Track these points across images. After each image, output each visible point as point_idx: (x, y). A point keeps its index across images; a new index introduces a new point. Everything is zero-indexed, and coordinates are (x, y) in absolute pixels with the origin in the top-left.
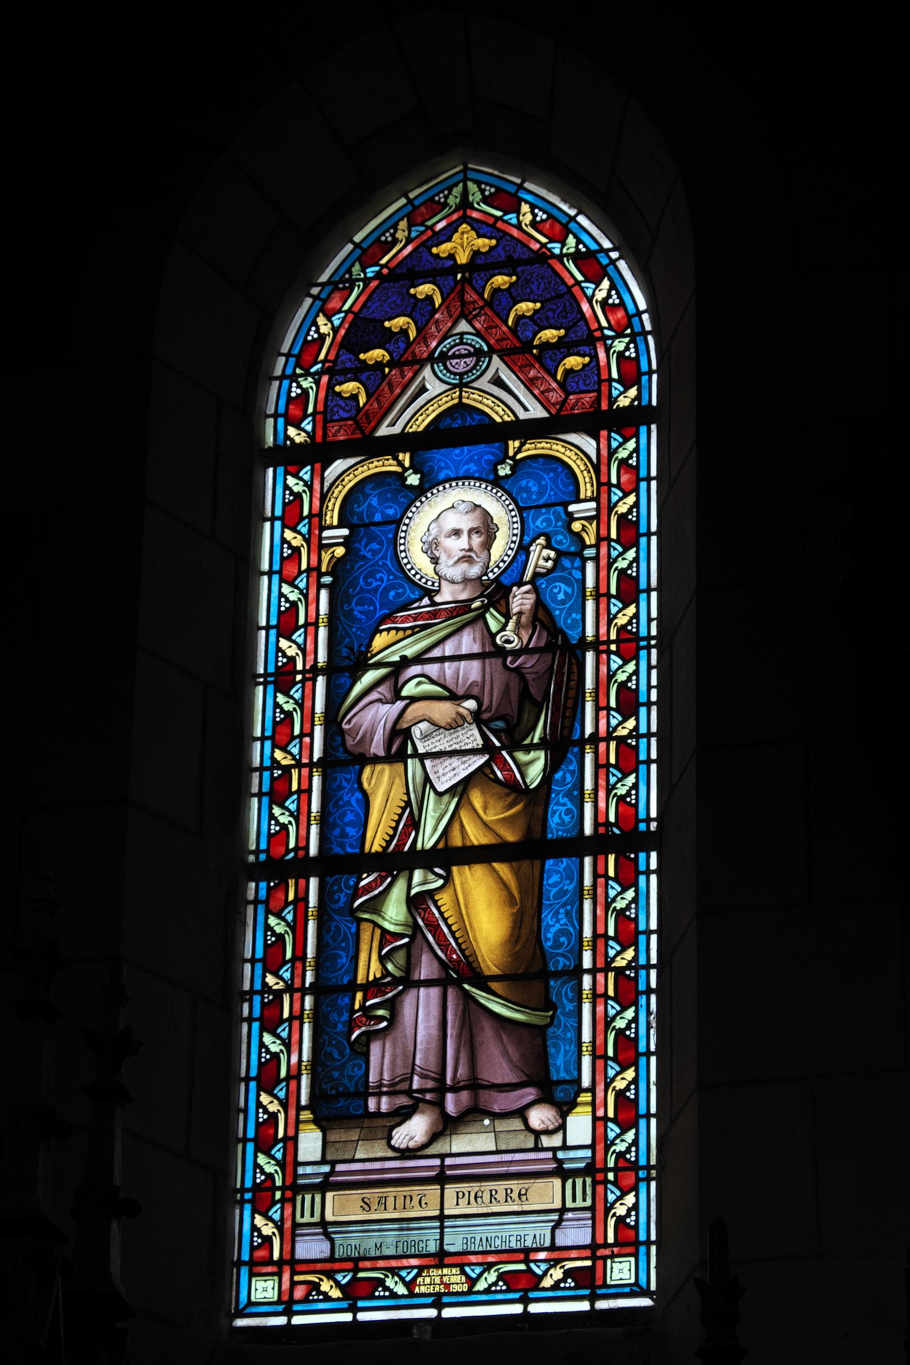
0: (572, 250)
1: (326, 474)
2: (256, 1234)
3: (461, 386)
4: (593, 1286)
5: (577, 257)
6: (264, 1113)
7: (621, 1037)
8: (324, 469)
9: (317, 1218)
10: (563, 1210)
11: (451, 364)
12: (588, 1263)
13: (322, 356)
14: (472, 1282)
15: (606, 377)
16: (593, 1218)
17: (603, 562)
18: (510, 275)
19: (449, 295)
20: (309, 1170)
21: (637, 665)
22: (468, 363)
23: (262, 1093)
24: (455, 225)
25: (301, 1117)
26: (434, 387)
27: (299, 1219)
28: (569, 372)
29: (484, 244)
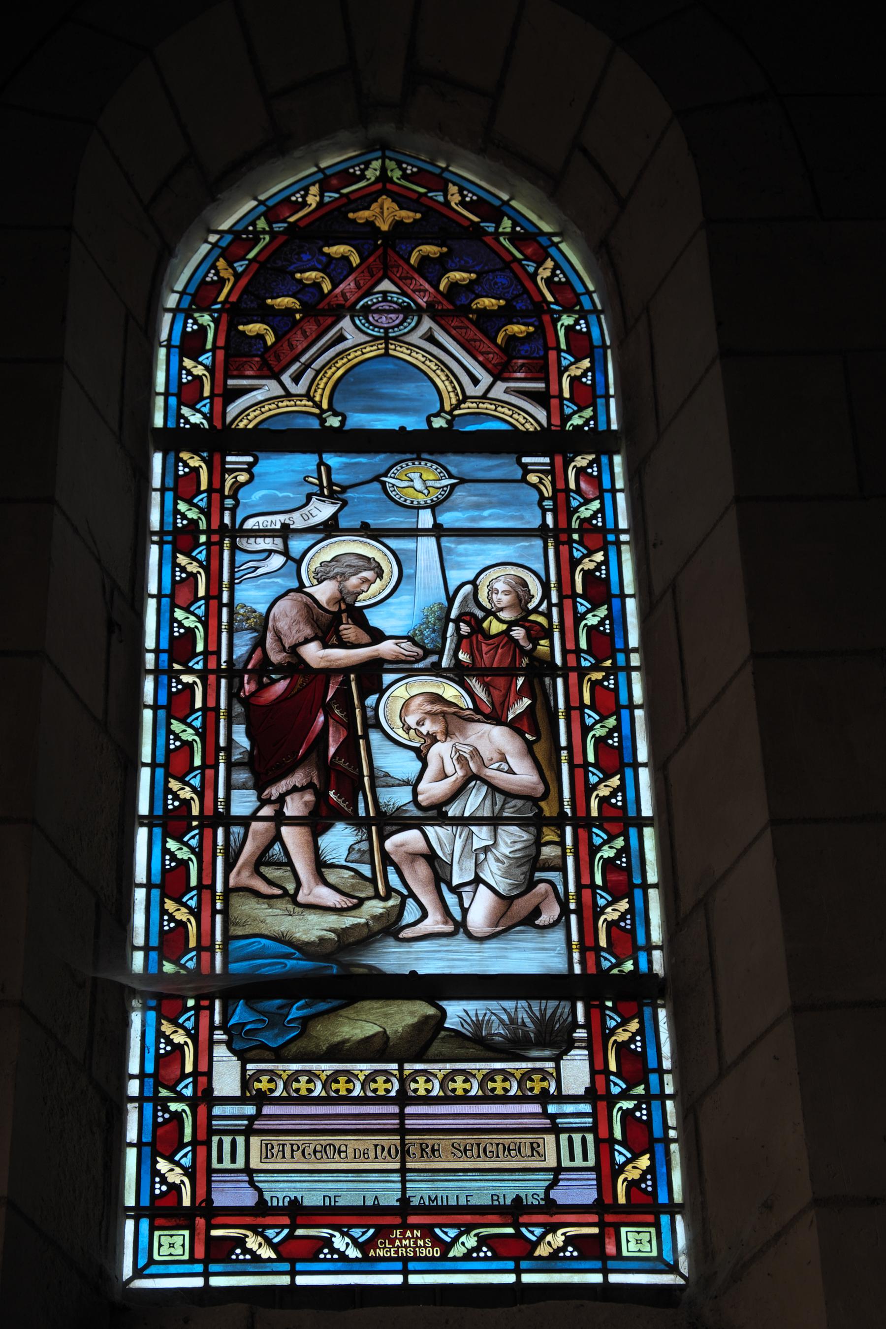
0: (509, 230)
1: (229, 409)
2: (170, 797)
3: (387, 339)
4: (604, 1257)
5: (513, 237)
6: (167, 1044)
7: (634, 1189)
8: (226, 404)
9: (240, 1163)
10: (558, 1170)
11: (373, 318)
12: (595, 1230)
13: (222, 298)
14: (447, 1247)
15: (592, 944)
16: (599, 1179)
17: (588, 913)
18: (441, 246)
19: (370, 255)
20: (229, 1110)
21: (595, 411)
22: (394, 319)
23: (166, 900)
24: (374, 196)
25: (215, 1037)
26: (353, 337)
27: (215, 1165)
28: (512, 339)
29: (408, 216)
